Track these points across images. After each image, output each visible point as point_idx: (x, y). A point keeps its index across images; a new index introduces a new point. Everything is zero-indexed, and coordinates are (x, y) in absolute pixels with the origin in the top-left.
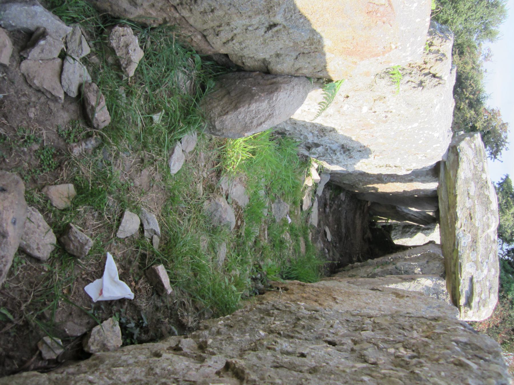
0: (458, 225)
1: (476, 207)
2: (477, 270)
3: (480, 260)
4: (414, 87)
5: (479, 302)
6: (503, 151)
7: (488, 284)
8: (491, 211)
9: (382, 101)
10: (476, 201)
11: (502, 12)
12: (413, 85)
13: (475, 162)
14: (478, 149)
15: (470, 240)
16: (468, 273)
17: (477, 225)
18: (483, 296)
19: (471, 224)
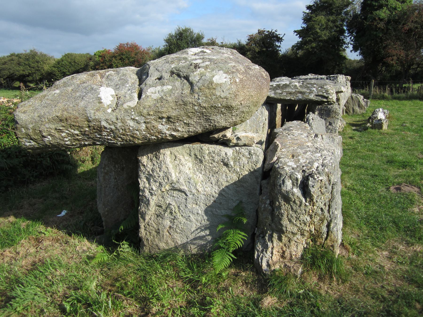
6: (277, 33)
7: (320, 88)
11: (186, 30)
16: (313, 97)
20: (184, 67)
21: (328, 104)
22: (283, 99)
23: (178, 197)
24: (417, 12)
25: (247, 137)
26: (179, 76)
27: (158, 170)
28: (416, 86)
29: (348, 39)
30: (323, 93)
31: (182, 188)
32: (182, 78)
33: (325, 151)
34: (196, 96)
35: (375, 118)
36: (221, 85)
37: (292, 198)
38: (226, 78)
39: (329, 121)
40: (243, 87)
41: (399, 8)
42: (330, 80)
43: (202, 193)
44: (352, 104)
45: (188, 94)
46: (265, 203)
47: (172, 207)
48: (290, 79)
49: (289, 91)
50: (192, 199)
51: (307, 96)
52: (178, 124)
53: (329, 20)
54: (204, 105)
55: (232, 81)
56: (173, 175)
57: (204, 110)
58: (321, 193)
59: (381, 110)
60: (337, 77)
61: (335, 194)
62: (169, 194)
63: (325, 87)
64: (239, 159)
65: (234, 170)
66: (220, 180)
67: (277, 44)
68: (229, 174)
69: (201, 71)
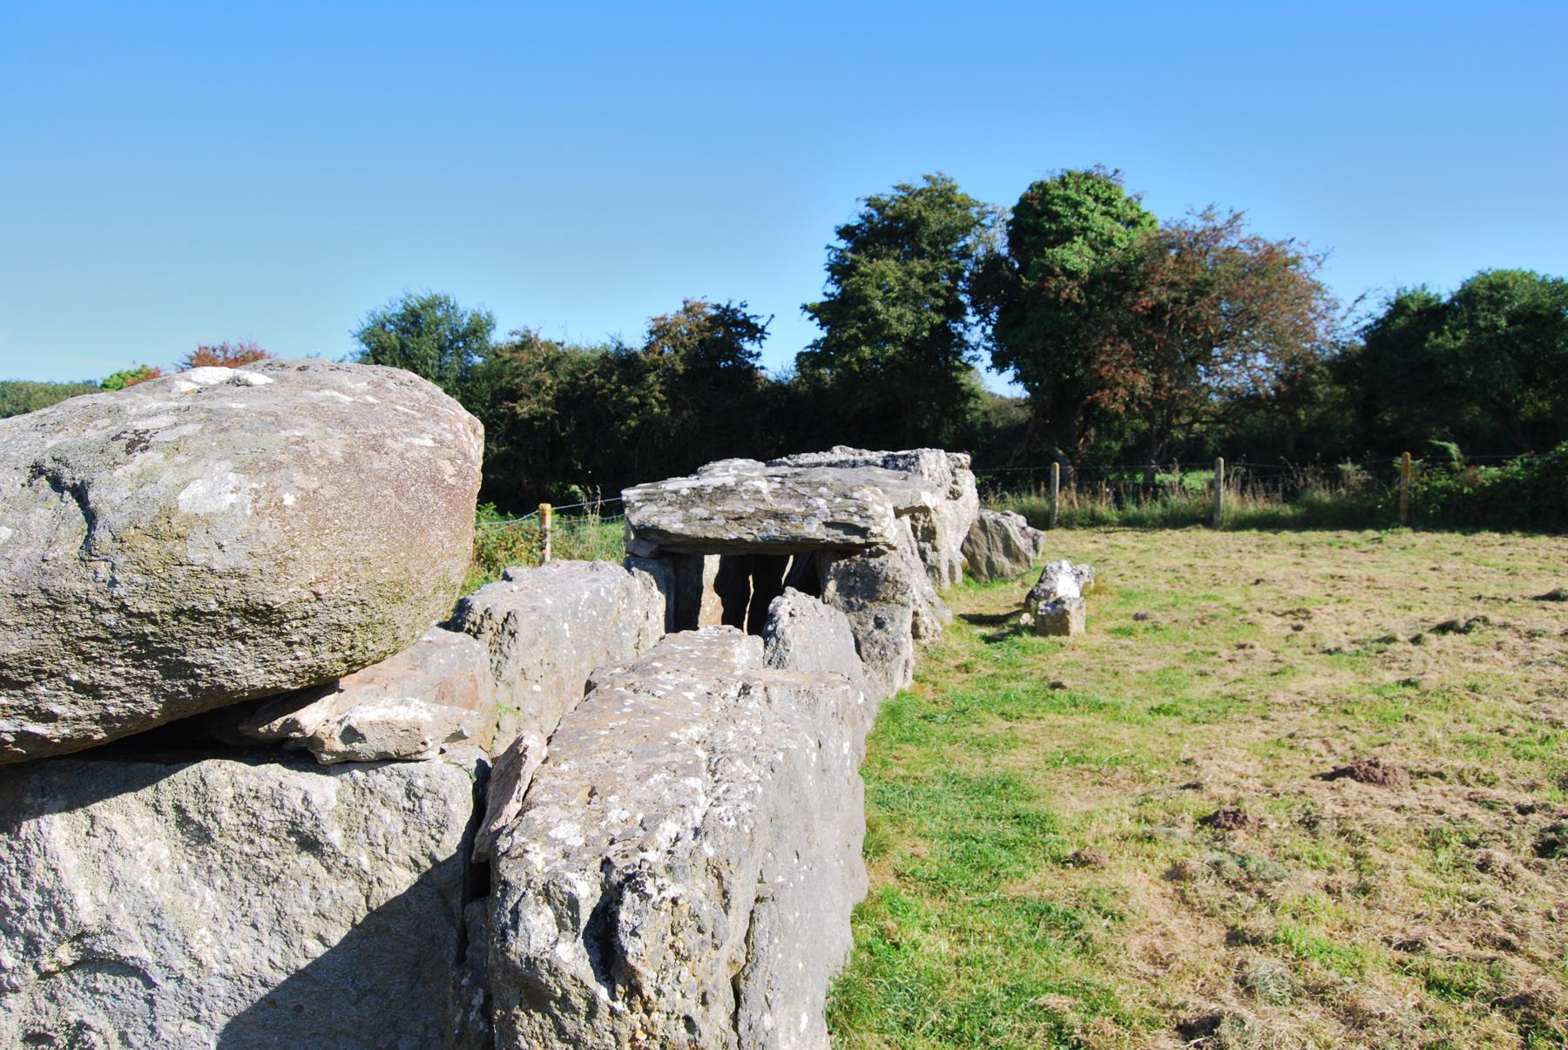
0: (749, 538)
6: (749, 312)
7: (839, 500)
11: (433, 304)
16: (818, 529)
18: (852, 509)
20: (85, 448)
23: (118, 992)
24: (1173, 252)
25: (388, 724)
26: (57, 484)
27: (17, 881)
29: (975, 331)
31: (126, 951)
32: (67, 494)
34: (104, 570)
35: (1048, 593)
36: (207, 522)
37: (551, 983)
38: (236, 490)
40: (318, 528)
41: (1121, 240)
42: (896, 467)
43: (217, 968)
44: (984, 545)
45: (70, 563)
46: (468, 1007)
47: (94, 1036)
48: (762, 464)
50: (176, 997)
52: (43, 689)
53: (910, 274)
54: (144, 607)
55: (262, 503)
56: (83, 899)
57: (149, 628)
58: (677, 953)
60: (917, 457)
61: (764, 943)
62: (76, 984)
63: (855, 495)
64: (366, 819)
65: (347, 864)
66: (288, 909)
67: (748, 346)
68: (328, 883)
69: (149, 464)
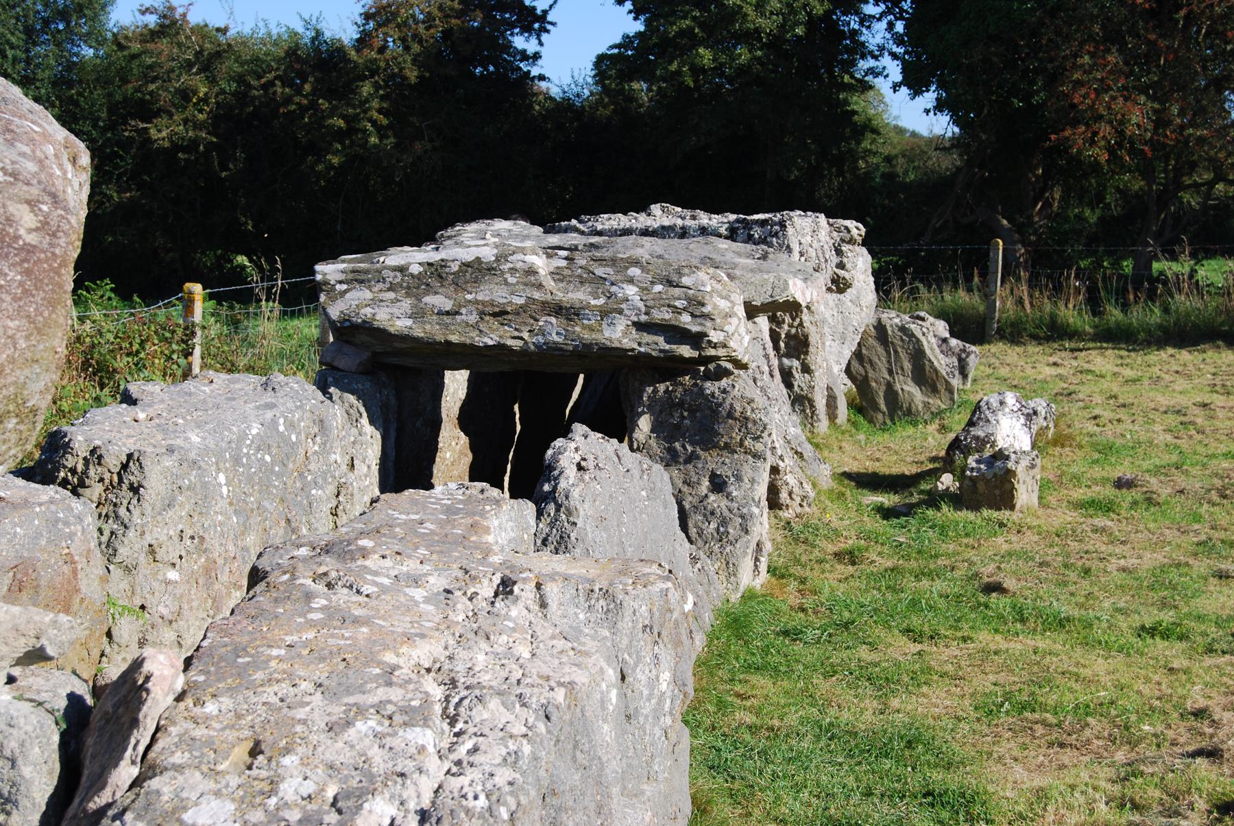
1: (480, 298)
2: (621, 312)
3: (601, 301)
4: (139, 500)
5: (692, 315)
7: (658, 288)
8: (497, 260)
9: (158, 550)
10: (469, 297)
12: (135, 501)
13: (381, 285)
14: (350, 276)
15: (553, 320)
16: (625, 334)
17: (521, 301)
19: (518, 314)
21: (708, 376)
22: (463, 345)
28: (1213, 271)
30: (677, 311)
33: (494, 703)
35: (982, 442)
39: (711, 466)
44: (882, 365)
49: (492, 303)
51: (591, 329)
59: (1010, 398)
60: (782, 225)
63: (686, 281)
